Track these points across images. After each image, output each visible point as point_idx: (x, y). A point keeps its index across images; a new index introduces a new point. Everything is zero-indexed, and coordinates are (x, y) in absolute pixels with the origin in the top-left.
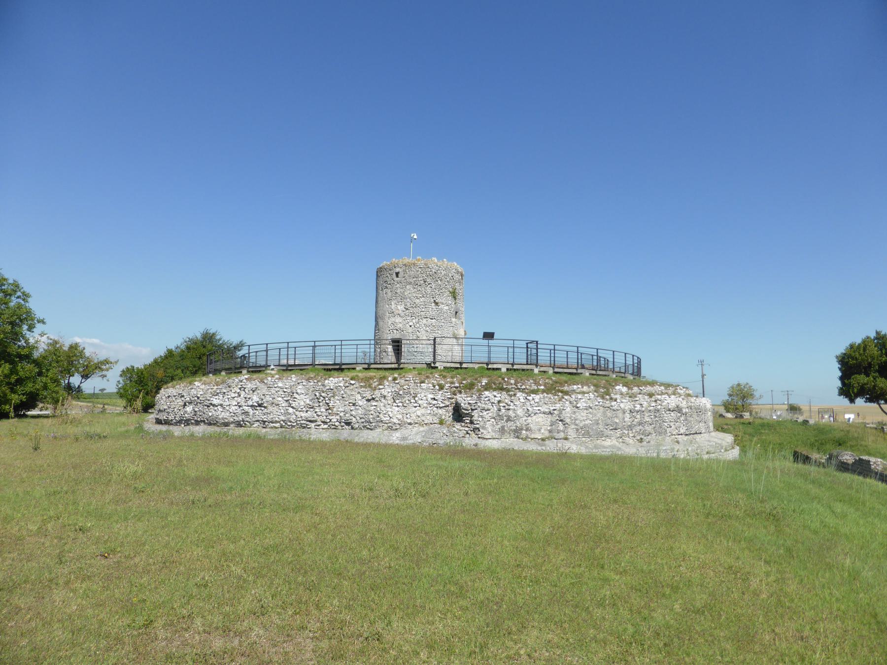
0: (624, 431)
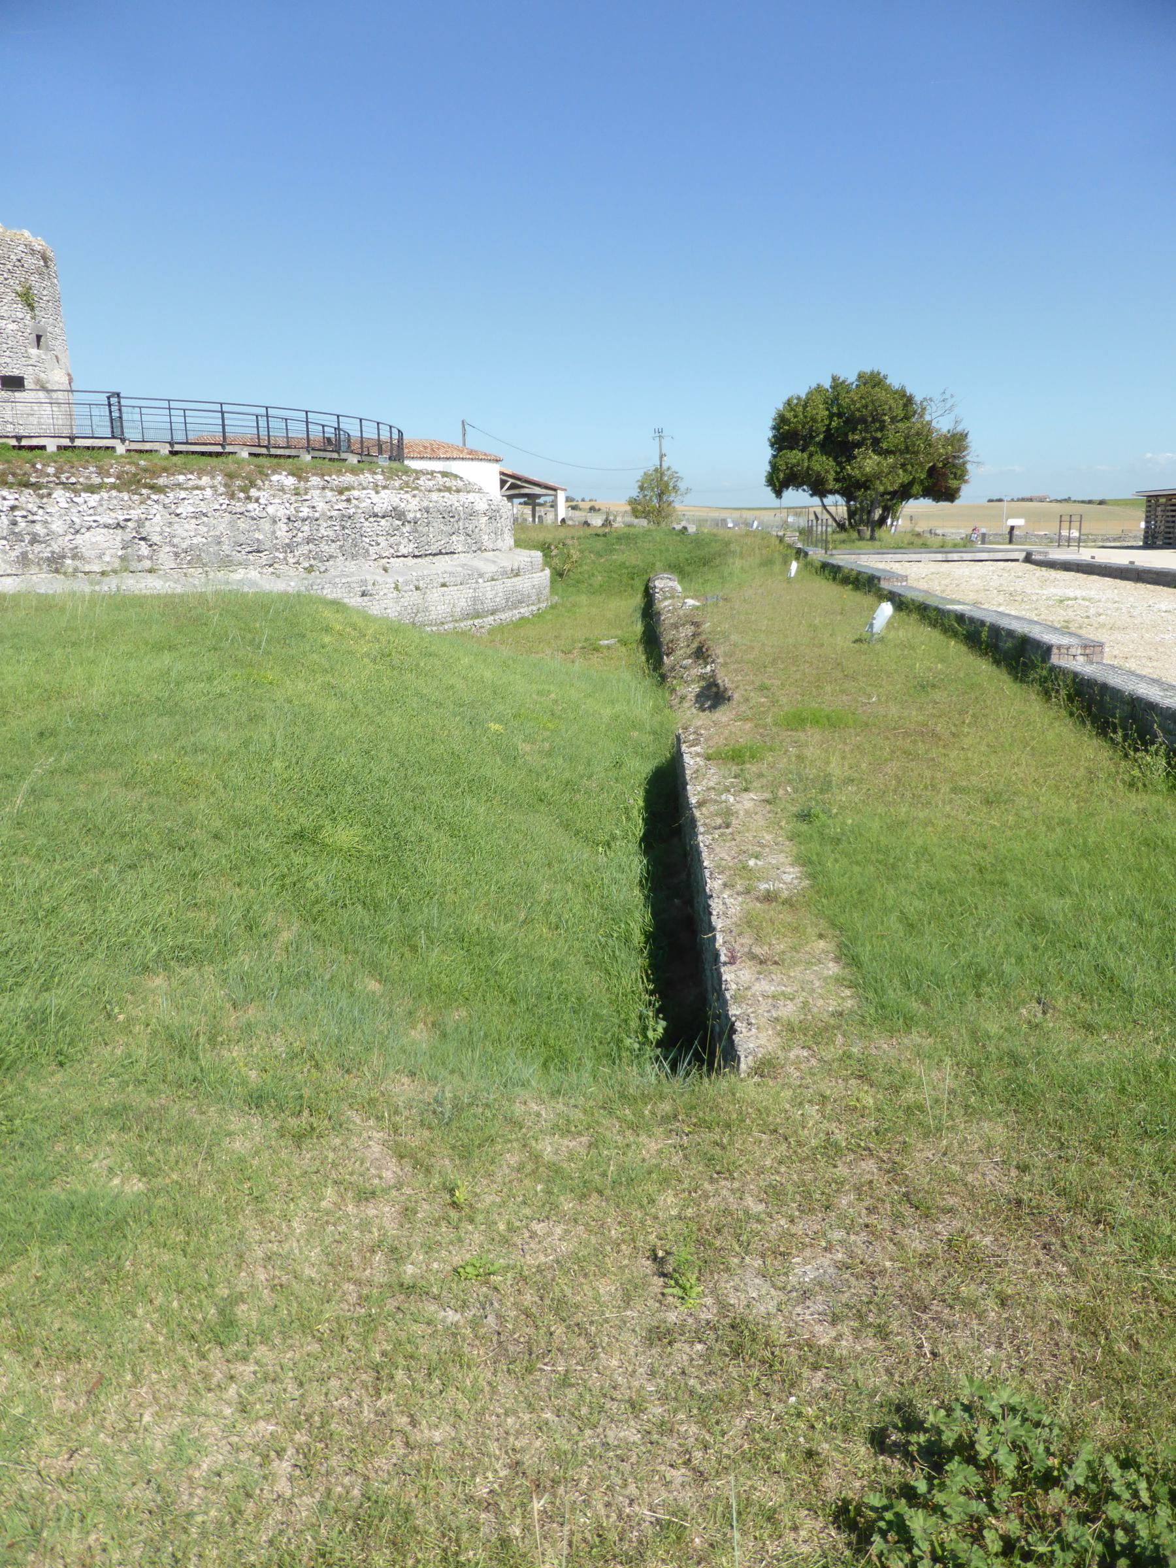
0: (277, 554)
